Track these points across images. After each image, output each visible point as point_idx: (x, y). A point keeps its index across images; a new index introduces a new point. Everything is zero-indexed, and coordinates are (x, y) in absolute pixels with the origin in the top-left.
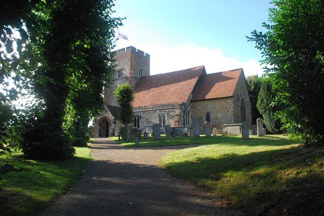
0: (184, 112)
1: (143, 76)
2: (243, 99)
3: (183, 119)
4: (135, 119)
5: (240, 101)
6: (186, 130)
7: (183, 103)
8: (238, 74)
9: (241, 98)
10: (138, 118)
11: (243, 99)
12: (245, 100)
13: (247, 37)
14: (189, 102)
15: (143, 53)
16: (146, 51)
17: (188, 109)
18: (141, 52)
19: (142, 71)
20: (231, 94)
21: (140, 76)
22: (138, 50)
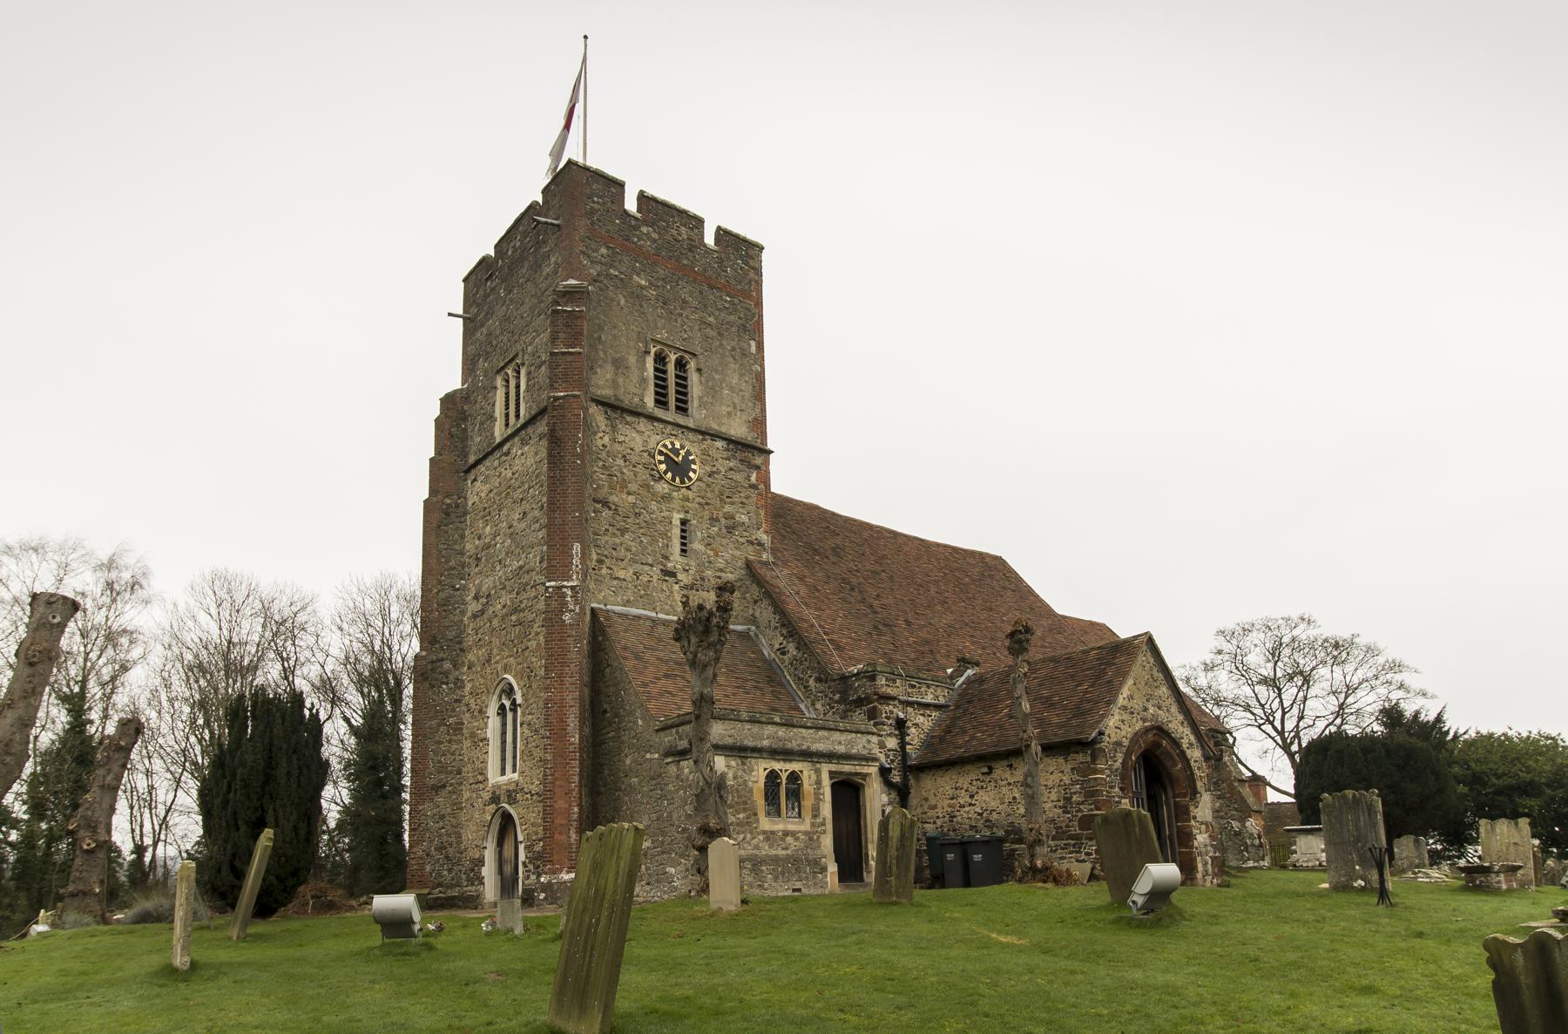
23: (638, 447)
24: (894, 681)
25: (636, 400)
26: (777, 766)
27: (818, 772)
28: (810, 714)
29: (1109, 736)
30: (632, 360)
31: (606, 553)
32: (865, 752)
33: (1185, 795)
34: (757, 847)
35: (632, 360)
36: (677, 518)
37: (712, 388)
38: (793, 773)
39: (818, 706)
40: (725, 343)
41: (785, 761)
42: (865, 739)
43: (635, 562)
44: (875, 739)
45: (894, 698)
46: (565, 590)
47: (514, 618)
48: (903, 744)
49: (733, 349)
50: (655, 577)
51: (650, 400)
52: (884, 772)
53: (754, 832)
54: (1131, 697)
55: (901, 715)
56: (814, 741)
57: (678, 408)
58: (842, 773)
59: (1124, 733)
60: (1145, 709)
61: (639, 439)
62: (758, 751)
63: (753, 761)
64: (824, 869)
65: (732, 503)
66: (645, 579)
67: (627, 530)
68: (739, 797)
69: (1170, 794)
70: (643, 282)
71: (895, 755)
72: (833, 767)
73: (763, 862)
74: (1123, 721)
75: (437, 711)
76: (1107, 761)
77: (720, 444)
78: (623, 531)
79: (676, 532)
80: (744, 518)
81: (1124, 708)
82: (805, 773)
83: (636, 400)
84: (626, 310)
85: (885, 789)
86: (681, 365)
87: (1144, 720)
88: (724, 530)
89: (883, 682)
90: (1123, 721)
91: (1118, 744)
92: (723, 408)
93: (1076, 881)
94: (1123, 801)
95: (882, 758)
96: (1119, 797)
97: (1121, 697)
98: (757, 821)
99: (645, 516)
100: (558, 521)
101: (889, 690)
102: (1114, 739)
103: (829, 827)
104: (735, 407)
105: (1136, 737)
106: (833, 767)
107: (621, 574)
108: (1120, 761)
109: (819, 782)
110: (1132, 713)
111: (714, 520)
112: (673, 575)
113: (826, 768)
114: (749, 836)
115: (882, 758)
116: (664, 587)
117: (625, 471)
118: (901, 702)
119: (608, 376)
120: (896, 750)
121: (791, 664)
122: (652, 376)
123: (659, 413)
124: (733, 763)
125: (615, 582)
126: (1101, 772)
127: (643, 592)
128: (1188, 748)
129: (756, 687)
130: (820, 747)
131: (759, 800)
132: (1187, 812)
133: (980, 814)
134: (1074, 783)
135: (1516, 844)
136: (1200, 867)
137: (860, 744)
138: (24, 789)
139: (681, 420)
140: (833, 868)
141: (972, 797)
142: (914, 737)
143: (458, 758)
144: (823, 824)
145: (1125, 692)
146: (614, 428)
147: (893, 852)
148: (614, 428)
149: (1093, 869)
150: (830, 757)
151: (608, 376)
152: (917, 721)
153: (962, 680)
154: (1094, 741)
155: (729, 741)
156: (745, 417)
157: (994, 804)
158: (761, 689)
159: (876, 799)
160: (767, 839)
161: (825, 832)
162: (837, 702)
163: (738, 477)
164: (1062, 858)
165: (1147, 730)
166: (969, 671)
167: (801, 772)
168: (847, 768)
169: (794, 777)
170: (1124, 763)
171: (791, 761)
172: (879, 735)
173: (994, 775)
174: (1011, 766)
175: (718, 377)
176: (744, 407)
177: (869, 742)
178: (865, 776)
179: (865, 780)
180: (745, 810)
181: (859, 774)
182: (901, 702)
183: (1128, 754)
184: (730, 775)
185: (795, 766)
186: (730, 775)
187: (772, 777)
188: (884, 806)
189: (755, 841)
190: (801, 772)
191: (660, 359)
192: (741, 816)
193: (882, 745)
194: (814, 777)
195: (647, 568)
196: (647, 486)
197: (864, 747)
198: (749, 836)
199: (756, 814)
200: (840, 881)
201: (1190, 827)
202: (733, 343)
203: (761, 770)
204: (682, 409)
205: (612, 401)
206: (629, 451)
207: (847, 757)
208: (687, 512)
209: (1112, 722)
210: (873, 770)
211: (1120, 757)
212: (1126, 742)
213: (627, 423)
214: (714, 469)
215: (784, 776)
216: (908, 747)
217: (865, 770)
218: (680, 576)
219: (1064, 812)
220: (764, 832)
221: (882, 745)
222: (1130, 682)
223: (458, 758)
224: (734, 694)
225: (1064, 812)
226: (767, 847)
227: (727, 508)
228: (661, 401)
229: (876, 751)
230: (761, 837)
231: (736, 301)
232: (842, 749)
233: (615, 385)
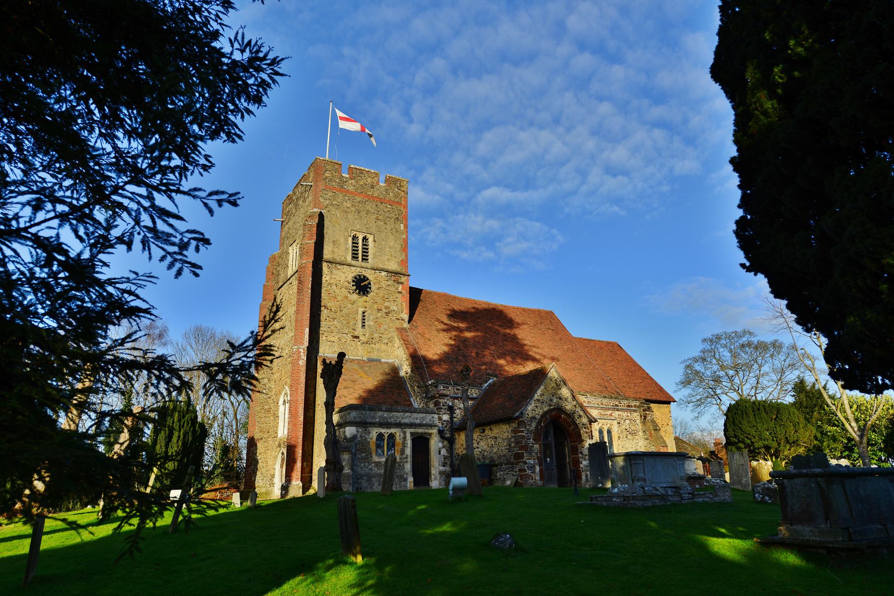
23: (343, 279)
24: (448, 388)
25: (343, 258)
26: (383, 431)
27: (405, 433)
28: (416, 405)
29: (528, 414)
30: (342, 240)
31: (325, 330)
32: (430, 423)
33: (576, 442)
34: (371, 469)
35: (342, 240)
36: (361, 310)
37: (381, 248)
38: (391, 433)
39: (418, 399)
40: (387, 227)
41: (387, 428)
42: (430, 416)
43: (339, 333)
44: (436, 416)
45: (447, 396)
46: (300, 350)
47: (289, 359)
48: (452, 418)
49: (392, 229)
50: (349, 339)
51: (349, 258)
52: (441, 432)
53: (370, 463)
54: (542, 395)
55: (450, 404)
56: (403, 418)
57: (363, 259)
58: (418, 433)
59: (537, 412)
60: (551, 400)
61: (343, 276)
62: (374, 425)
63: (371, 429)
64: (406, 480)
65: (389, 301)
66: (344, 340)
67: (335, 318)
68: (363, 446)
69: (569, 441)
70: (348, 205)
71: (447, 424)
72: (413, 430)
73: (374, 476)
74: (537, 407)
75: (260, 403)
76: (526, 427)
77: (384, 274)
78: (334, 319)
79: (360, 317)
80: (395, 308)
81: (538, 400)
82: (398, 434)
83: (343, 258)
84: (340, 219)
85: (442, 440)
86: (365, 239)
87: (550, 406)
88: (384, 314)
89: (442, 388)
90: (537, 407)
91: (534, 418)
92: (386, 257)
93: (337, 480)
94: (535, 446)
95: (440, 425)
96: (532, 444)
97: (536, 395)
98: (372, 457)
99: (345, 311)
100: (300, 318)
101: (445, 392)
102: (531, 415)
103: (409, 459)
104: (392, 256)
105: (545, 414)
106: (413, 430)
107: (332, 339)
108: (534, 426)
109: (405, 438)
110: (543, 402)
111: (379, 310)
112: (357, 337)
113: (408, 431)
114: (367, 464)
115: (440, 425)
116: (353, 344)
117: (336, 291)
118: (451, 398)
119: (330, 249)
120: (448, 421)
121: (409, 379)
122: (351, 246)
123: (354, 263)
124: (360, 430)
125: (329, 343)
126: (522, 432)
127: (342, 347)
128: (578, 418)
129: (389, 391)
130: (407, 421)
131: (373, 447)
132: (577, 449)
133: (481, 452)
134: (512, 437)
135: (742, 465)
136: (584, 477)
137: (428, 419)
138: (46, 510)
139: (364, 264)
140: (411, 479)
141: (478, 444)
142: (458, 414)
143: (268, 425)
144: (407, 458)
145: (539, 392)
146: (331, 272)
147: (388, 473)
148: (331, 272)
149: (517, 479)
150: (411, 425)
151: (330, 249)
152: (460, 406)
153: (486, 385)
154: (517, 417)
155: (358, 420)
156: (397, 260)
157: (486, 447)
158: (392, 392)
159: (435, 443)
160: (376, 466)
161: (407, 462)
162: (424, 398)
163: (392, 289)
164: (507, 474)
165: (550, 411)
166: (491, 380)
167: (395, 433)
168: (420, 431)
169: (392, 436)
170: (536, 427)
171: (390, 428)
172: (438, 414)
173: (485, 433)
174: (491, 429)
175: (383, 243)
176: (396, 255)
177: (433, 417)
178: (430, 434)
179: (431, 436)
180: (365, 452)
181: (427, 433)
182: (451, 398)
183: (539, 423)
184: (359, 436)
185: (393, 431)
186: (359, 436)
187: (380, 436)
188: (440, 448)
189: (370, 467)
190: (395, 433)
191: (355, 238)
192: (363, 455)
193: (440, 419)
194: (402, 436)
195: (344, 335)
196: (346, 297)
197: (430, 420)
198: (367, 464)
199: (371, 454)
200: (414, 486)
201: (578, 457)
202: (391, 227)
203: (375, 433)
204: (365, 259)
205: (332, 260)
206: (338, 282)
207: (420, 425)
208: (366, 307)
209: (530, 408)
210: (434, 431)
211: (534, 425)
212: (538, 417)
213: (338, 269)
214: (380, 286)
215: (386, 436)
216: (455, 419)
217: (430, 431)
218: (361, 338)
219: (509, 452)
220: (375, 462)
221: (440, 419)
222: (542, 387)
223: (268, 425)
224: (377, 395)
225: (509, 452)
226: (376, 469)
227: (387, 304)
228: (355, 257)
229: (437, 422)
230: (373, 465)
231: (394, 207)
232: (418, 421)
233: (333, 252)
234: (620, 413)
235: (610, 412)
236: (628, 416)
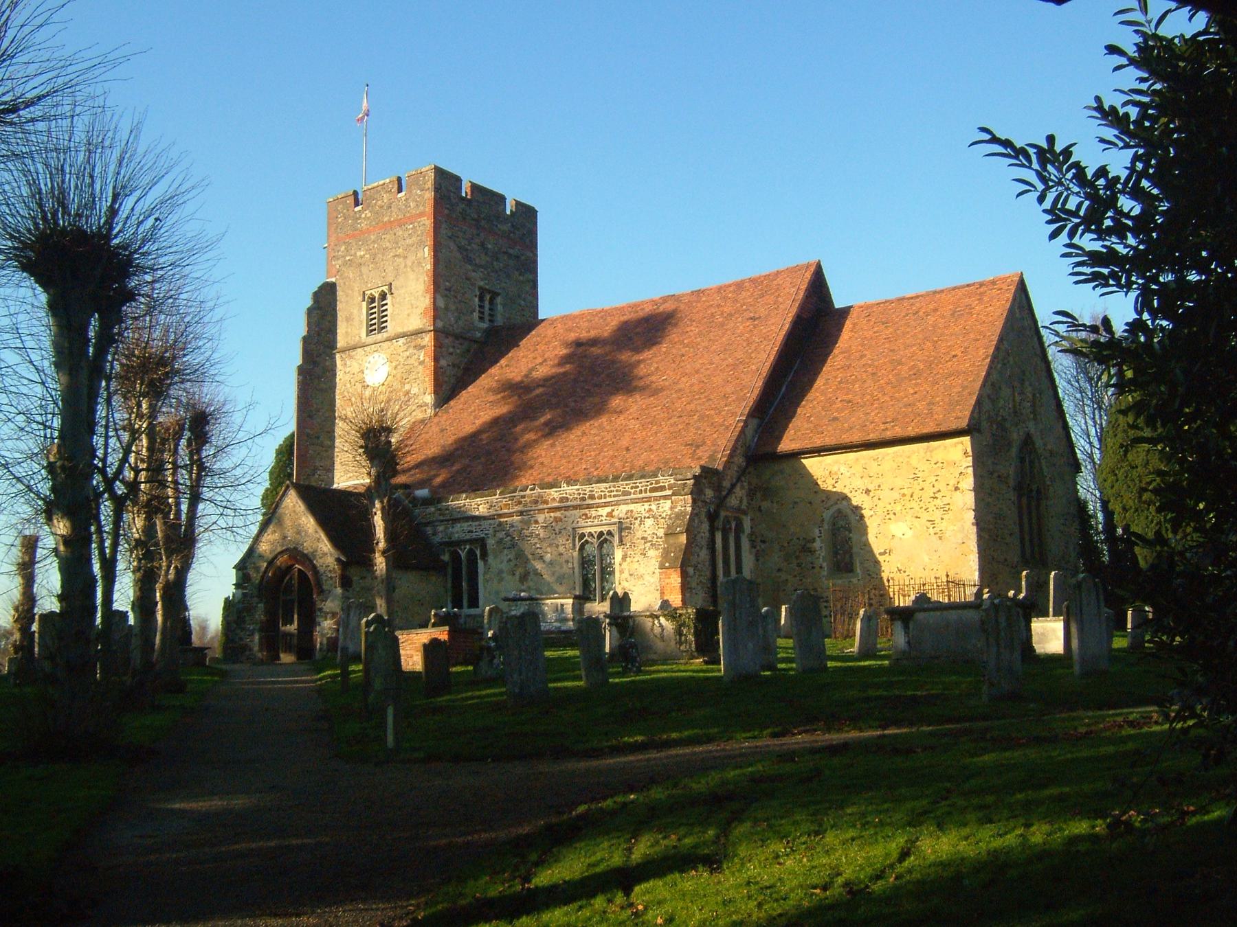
0: (712, 517)
1: (432, 328)
2: (1028, 440)
3: (704, 554)
4: (456, 557)
5: (1014, 451)
6: (1229, 19)
7: (704, 469)
8: (996, 311)
9: (1016, 436)
10: (471, 553)
11: (1028, 440)
12: (1039, 443)
13: (1101, 295)
14: (740, 460)
15: (502, 199)
16: (513, 192)
17: (733, 501)
18: (487, 199)
19: (494, 294)
20: (964, 424)
21: (484, 325)
22: (475, 188)
25: (357, 338)
227: (407, 387)
234: (631, 507)
235: (608, 509)
236: (650, 510)
